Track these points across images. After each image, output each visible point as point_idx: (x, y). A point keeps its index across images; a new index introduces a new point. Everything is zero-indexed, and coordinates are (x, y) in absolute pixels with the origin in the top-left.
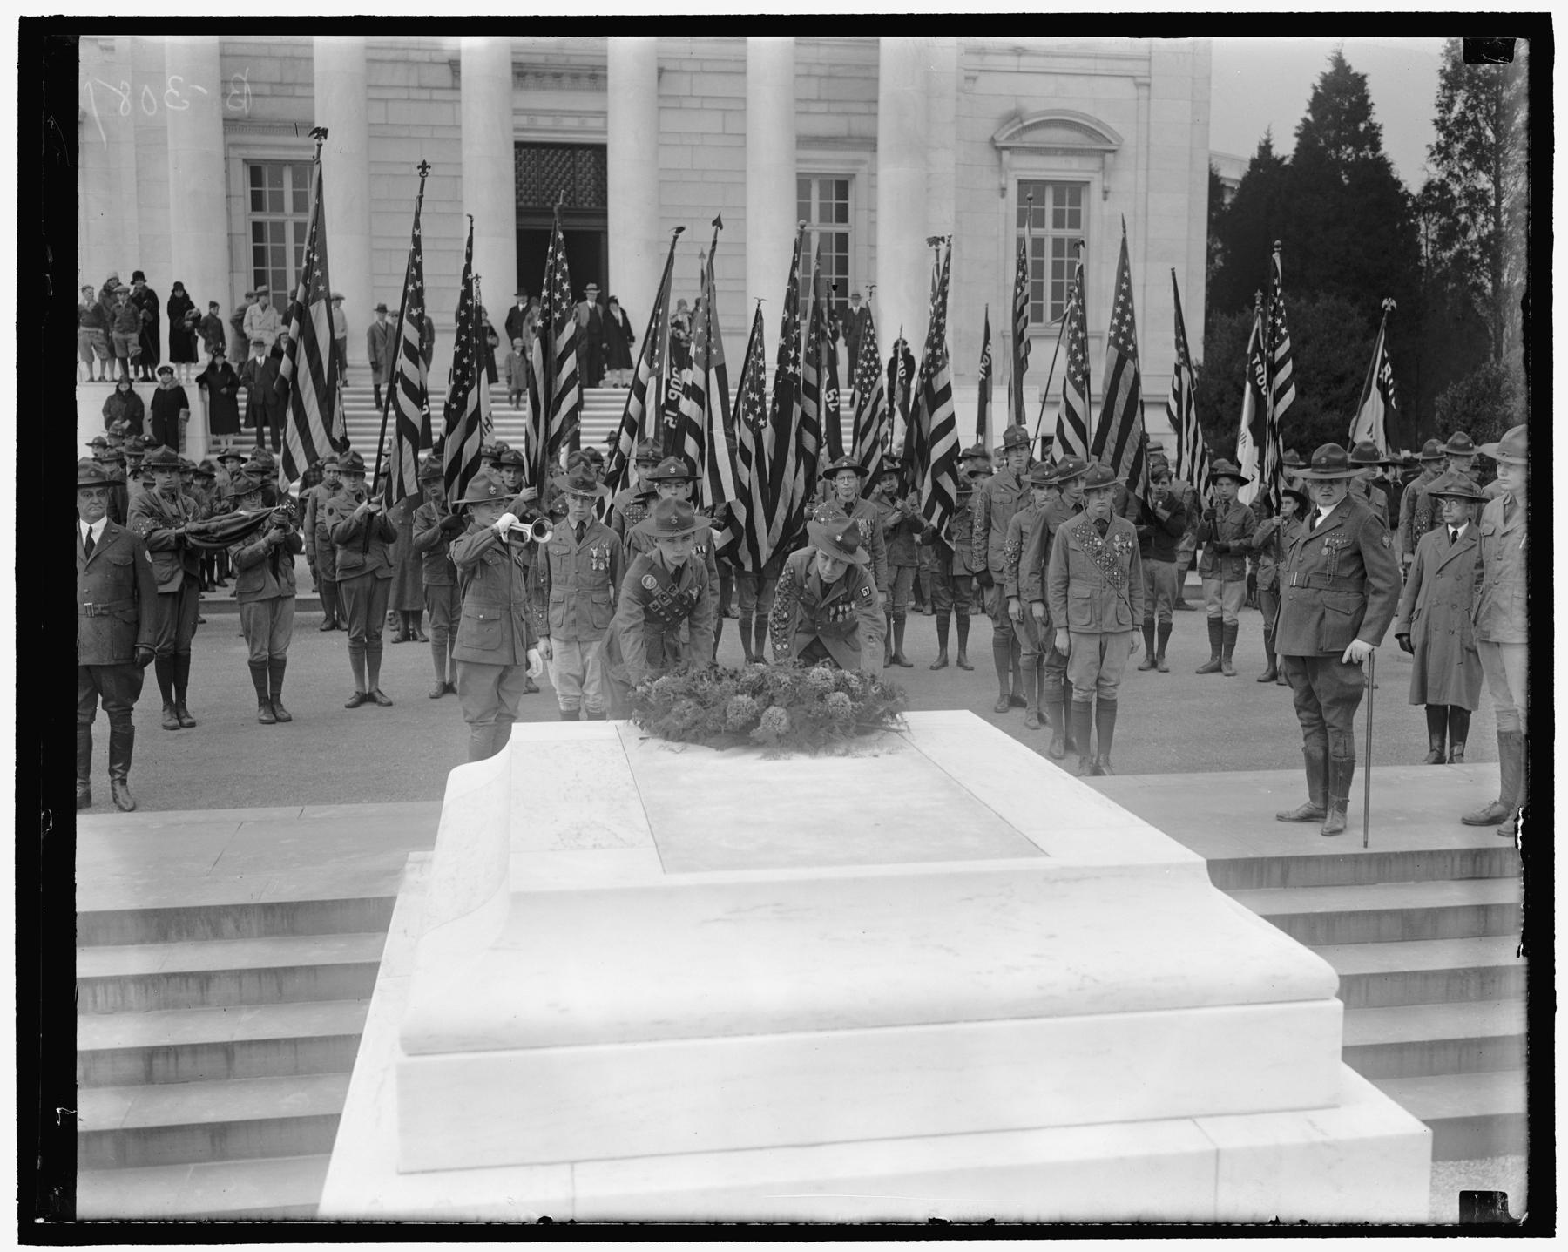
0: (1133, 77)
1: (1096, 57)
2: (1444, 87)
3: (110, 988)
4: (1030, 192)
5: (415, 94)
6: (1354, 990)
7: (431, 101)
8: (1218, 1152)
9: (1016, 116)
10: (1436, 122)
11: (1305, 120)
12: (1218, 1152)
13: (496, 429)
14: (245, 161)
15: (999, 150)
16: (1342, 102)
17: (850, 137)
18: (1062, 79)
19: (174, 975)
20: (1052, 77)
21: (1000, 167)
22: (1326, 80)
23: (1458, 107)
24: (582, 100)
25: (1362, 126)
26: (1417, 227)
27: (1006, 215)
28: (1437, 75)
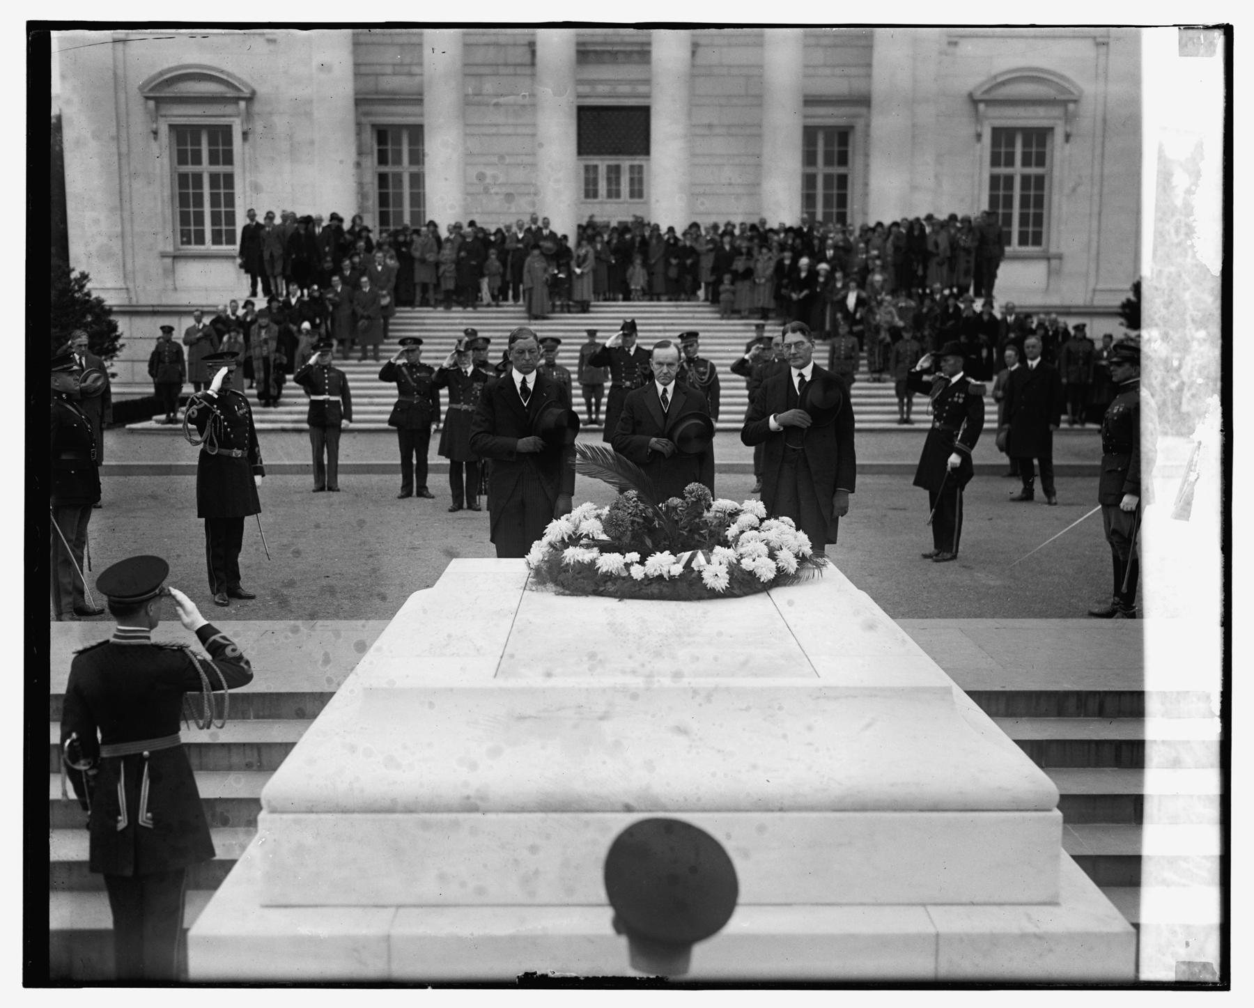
4: (1003, 137)
5: (502, 70)
6: (1068, 803)
7: (515, 75)
8: (937, 935)
12: (937, 935)
14: (373, 126)
21: (978, 118)
24: (629, 71)
27: (981, 156)
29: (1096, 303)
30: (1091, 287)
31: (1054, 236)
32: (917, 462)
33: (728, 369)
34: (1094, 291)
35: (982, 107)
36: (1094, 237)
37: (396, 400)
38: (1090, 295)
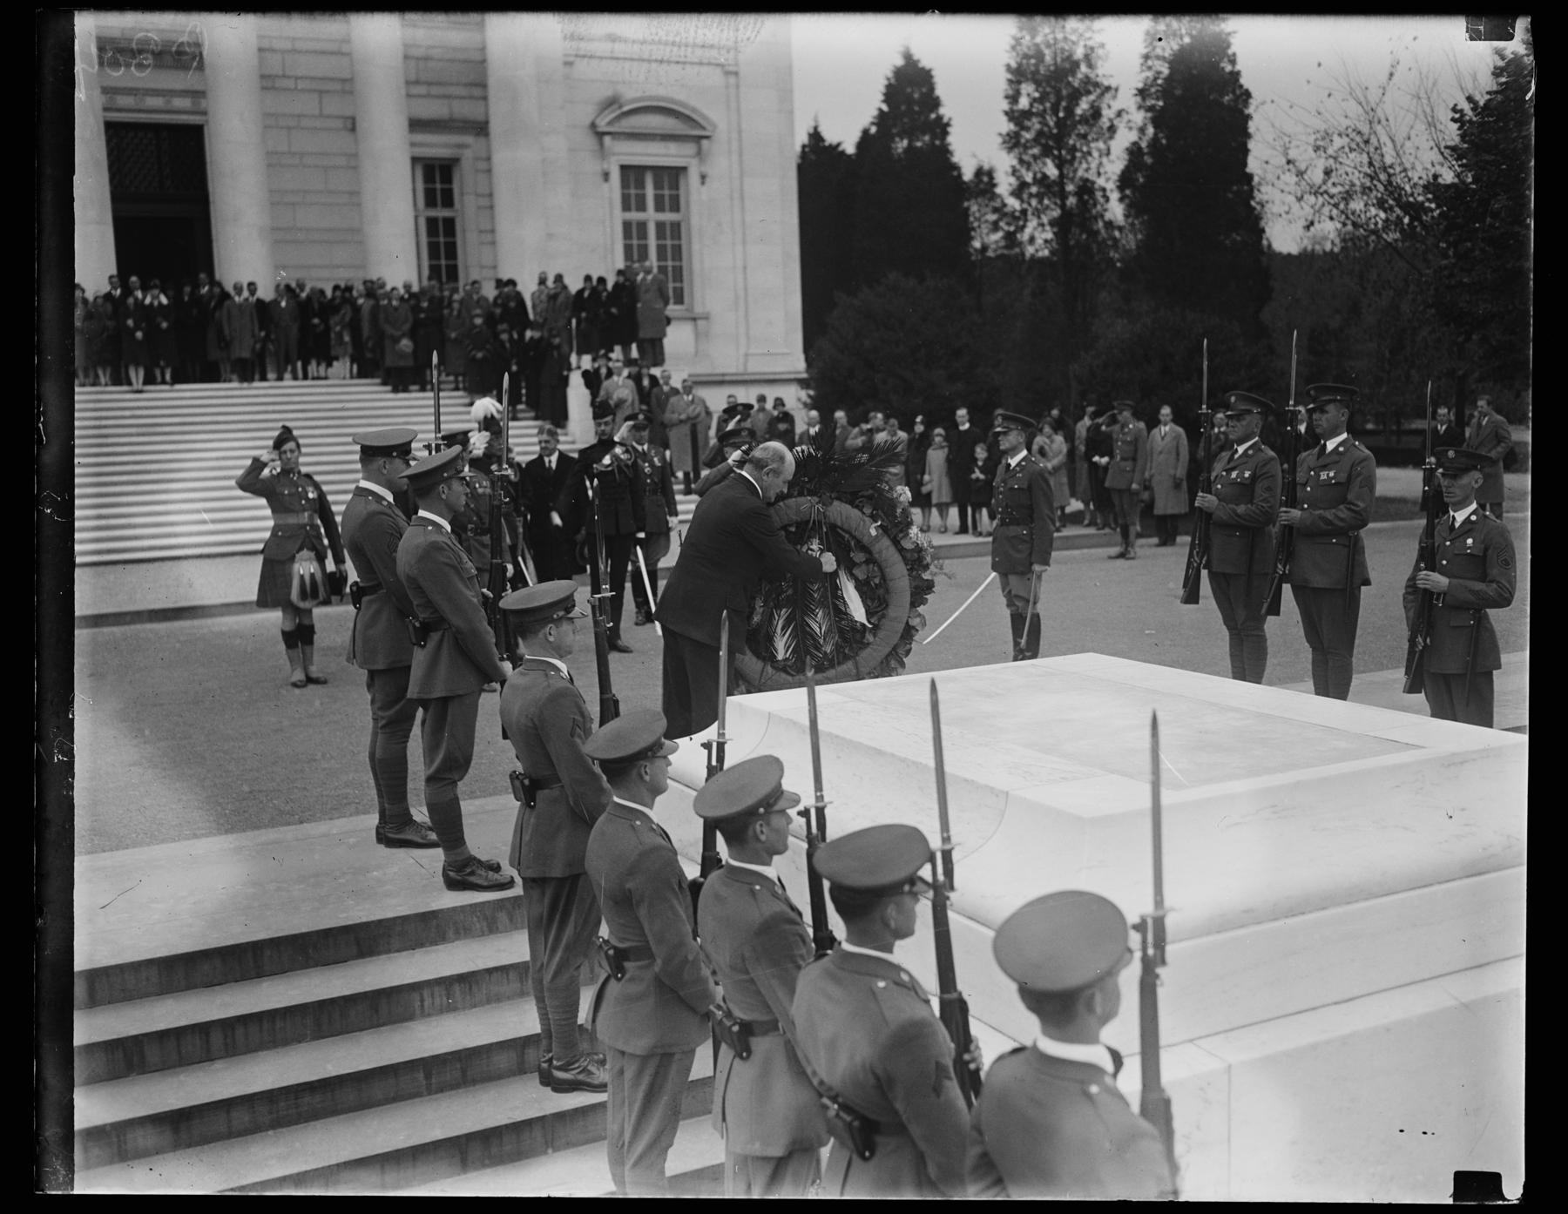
2: (1010, 81)
3: (436, 989)
4: (632, 174)
9: (612, 102)
10: (1006, 113)
11: (880, 110)
13: (536, 440)
15: (601, 135)
16: (911, 95)
17: (452, 120)
19: (496, 969)
22: (898, 72)
23: (1024, 103)
25: (933, 116)
26: (968, 209)
28: (1003, 69)
30: (742, 351)
32: (1054, 554)
33: (233, 483)
34: (746, 355)
35: (607, 139)
36: (741, 293)
37: (271, 523)
38: (742, 360)
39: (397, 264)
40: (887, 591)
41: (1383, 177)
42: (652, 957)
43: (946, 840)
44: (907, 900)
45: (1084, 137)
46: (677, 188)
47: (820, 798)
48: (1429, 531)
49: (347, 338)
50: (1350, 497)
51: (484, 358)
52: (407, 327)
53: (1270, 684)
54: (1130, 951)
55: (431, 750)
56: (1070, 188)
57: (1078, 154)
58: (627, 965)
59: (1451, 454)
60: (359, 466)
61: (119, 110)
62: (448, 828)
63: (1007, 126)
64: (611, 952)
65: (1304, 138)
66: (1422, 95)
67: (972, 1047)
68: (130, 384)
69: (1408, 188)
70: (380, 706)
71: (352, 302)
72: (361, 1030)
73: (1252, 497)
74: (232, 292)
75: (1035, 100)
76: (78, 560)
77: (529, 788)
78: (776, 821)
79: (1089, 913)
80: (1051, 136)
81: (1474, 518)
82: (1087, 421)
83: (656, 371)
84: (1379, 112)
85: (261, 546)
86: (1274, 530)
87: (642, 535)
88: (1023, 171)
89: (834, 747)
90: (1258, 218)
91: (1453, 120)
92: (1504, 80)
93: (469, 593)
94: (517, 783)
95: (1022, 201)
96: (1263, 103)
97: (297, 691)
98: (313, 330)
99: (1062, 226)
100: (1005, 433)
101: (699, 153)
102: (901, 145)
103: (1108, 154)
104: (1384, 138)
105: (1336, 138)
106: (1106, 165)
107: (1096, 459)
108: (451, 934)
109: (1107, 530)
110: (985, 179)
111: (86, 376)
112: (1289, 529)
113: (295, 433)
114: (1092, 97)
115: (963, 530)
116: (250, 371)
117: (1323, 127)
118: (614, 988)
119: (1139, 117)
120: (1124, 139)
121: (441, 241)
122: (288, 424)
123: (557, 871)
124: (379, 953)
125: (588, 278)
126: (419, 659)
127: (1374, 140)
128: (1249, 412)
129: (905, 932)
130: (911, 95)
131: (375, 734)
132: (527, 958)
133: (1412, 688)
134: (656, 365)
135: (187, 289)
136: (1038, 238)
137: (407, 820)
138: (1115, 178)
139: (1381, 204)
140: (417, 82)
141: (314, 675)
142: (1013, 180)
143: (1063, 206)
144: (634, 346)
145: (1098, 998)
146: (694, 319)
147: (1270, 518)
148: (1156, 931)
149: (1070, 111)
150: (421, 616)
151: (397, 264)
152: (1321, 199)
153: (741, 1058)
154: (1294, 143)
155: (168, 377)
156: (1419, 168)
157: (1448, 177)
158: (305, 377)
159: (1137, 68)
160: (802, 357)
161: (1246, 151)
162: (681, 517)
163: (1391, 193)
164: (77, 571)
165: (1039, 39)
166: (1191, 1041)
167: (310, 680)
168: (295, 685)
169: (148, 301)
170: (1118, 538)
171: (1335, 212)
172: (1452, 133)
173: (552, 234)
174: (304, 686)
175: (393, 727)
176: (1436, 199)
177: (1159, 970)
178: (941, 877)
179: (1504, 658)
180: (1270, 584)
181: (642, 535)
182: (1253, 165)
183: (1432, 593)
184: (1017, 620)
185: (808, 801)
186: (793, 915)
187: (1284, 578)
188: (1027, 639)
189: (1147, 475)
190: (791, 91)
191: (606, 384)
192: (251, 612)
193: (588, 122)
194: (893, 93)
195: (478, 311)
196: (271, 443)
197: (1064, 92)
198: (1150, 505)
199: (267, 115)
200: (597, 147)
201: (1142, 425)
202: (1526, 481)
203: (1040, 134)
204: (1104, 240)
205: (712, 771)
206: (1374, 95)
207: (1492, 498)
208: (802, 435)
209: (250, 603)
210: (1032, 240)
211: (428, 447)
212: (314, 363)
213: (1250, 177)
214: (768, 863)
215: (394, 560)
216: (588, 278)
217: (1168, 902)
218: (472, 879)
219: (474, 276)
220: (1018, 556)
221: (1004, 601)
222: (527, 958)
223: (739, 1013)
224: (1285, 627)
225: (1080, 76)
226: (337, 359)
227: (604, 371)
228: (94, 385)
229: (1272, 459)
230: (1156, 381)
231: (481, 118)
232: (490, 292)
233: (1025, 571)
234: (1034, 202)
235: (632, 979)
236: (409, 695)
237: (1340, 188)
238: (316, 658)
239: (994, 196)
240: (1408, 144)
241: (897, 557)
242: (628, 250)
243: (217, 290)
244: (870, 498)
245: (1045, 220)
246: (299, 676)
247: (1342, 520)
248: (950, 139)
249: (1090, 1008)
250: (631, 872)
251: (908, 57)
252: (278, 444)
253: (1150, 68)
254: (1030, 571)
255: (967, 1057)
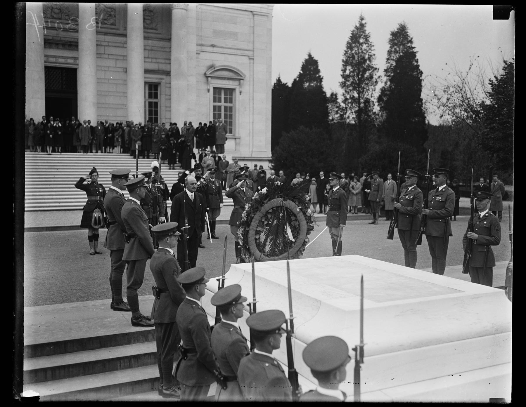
0: (248, 56)
1: (237, 49)
2: (343, 65)
4: (217, 91)
9: (212, 67)
10: (342, 75)
11: (300, 73)
15: (207, 77)
17: (159, 70)
18: (226, 55)
20: (223, 55)
21: (207, 82)
22: (306, 61)
23: (348, 72)
26: (328, 106)
29: (253, 156)
30: (251, 150)
31: (237, 130)
35: (209, 79)
36: (251, 131)
37: (87, 200)
38: (250, 153)
39: (137, 116)
40: (300, 230)
41: (466, 101)
42: (196, 352)
43: (291, 316)
44: (277, 336)
45: (367, 84)
46: (232, 96)
47: (254, 300)
48: (472, 219)
49: (120, 140)
50: (446, 206)
51: (165, 148)
52: (140, 137)
53: (419, 268)
54: (349, 357)
55: (129, 278)
56: (362, 101)
57: (365, 90)
58: (188, 355)
59: (479, 193)
60: (111, 182)
61: (59, 63)
62: (134, 305)
63: (342, 80)
64: (183, 350)
65: (440, 87)
66: (480, 75)
67: (299, 389)
68: (47, 152)
69: (475, 105)
70: (114, 262)
71: (122, 128)
72: (99, 373)
73: (413, 204)
74: (83, 124)
75: (351, 72)
76: (26, 209)
77: (158, 292)
78: (239, 306)
79: (338, 343)
80: (356, 84)
81: (487, 215)
82: (364, 178)
83: (221, 155)
84: (466, 80)
85: (82, 208)
86: (420, 216)
87: (208, 209)
88: (347, 95)
89: (263, 284)
90: (424, 113)
91: (489, 84)
92: (507, 71)
93: (145, 226)
94: (154, 290)
95: (346, 104)
96: (428, 76)
97: (91, 256)
98: (107, 137)
99: (359, 113)
100: (332, 180)
101: (240, 84)
102: (306, 85)
103: (375, 90)
104: (467, 89)
105: (451, 88)
106: (374, 93)
107: (366, 190)
108: (132, 341)
109: (369, 214)
110: (334, 97)
111: (33, 149)
112: (425, 216)
113: (97, 170)
114: (370, 71)
115: (321, 212)
116: (87, 149)
117: (447, 85)
118: (183, 363)
119: (385, 79)
120: (380, 85)
121: (153, 110)
122: (96, 167)
123: (166, 321)
124: (108, 347)
125: (200, 123)
126: (127, 246)
127: (464, 89)
128: (413, 176)
129: (277, 347)
130: (310, 68)
131: (112, 272)
132: (156, 351)
133: (465, 272)
134: (221, 153)
135: (68, 122)
136: (351, 117)
137: (122, 301)
138: (376, 98)
139: (466, 110)
140: (148, 58)
141: (98, 251)
142: (343, 97)
143: (359, 107)
144: (214, 146)
145: (338, 374)
146: (235, 139)
147: (418, 211)
148: (360, 351)
149: (363, 76)
150: (128, 232)
151: (137, 116)
152: (445, 108)
153: (224, 389)
154: (437, 89)
155: (60, 151)
156: (479, 99)
157: (488, 102)
158: (105, 152)
159: (385, 63)
160: (271, 152)
161: (421, 91)
162: (224, 204)
163: (469, 107)
164: (25, 213)
165: (353, 52)
166: (380, 390)
167: (96, 253)
168: (91, 254)
169: (55, 125)
170: (372, 217)
171: (450, 112)
172: (489, 88)
173: (188, 107)
174: (94, 254)
175: (118, 269)
176: (483, 109)
177: (361, 365)
178: (289, 328)
179: (497, 263)
180: (419, 234)
181: (208, 209)
182: (423, 96)
183: (472, 240)
184: (334, 243)
185: (250, 300)
186: (243, 339)
187: (423, 232)
188: (338, 249)
189: (383, 196)
190: (271, 66)
191: (204, 158)
192: (78, 229)
193: (204, 72)
194: (304, 67)
195: (164, 133)
196: (89, 173)
197: (361, 69)
198: (384, 206)
199: (97, 66)
200: (206, 81)
201: (382, 180)
202: (512, 203)
203: (352, 83)
204: (373, 119)
205: (219, 288)
206: (464, 75)
207: (496, 210)
208: (269, 178)
209: (78, 226)
210: (348, 117)
211: (134, 175)
212: (108, 148)
213: (422, 100)
214: (236, 321)
215: (121, 213)
216: (200, 123)
217: (365, 342)
218: (141, 323)
219: (163, 121)
220: (336, 222)
221: (330, 236)
222: (156, 351)
223: (223, 373)
224: (423, 249)
225: (366, 64)
226: (116, 147)
227: (204, 154)
228: (35, 152)
229: (420, 192)
230: (384, 166)
231: (169, 70)
232: (168, 127)
233: (337, 226)
234: (350, 105)
235: (189, 360)
236: (123, 259)
237: (452, 105)
238: (99, 244)
239: (337, 103)
240: (475, 91)
241: (304, 219)
242: (214, 115)
243: (77, 122)
244: (299, 199)
245: (353, 111)
246: (92, 251)
247: (442, 213)
248: (323, 83)
249: (335, 377)
250: (191, 322)
251: (310, 56)
252: (91, 173)
253: (389, 63)
254: (339, 226)
255: (297, 392)
